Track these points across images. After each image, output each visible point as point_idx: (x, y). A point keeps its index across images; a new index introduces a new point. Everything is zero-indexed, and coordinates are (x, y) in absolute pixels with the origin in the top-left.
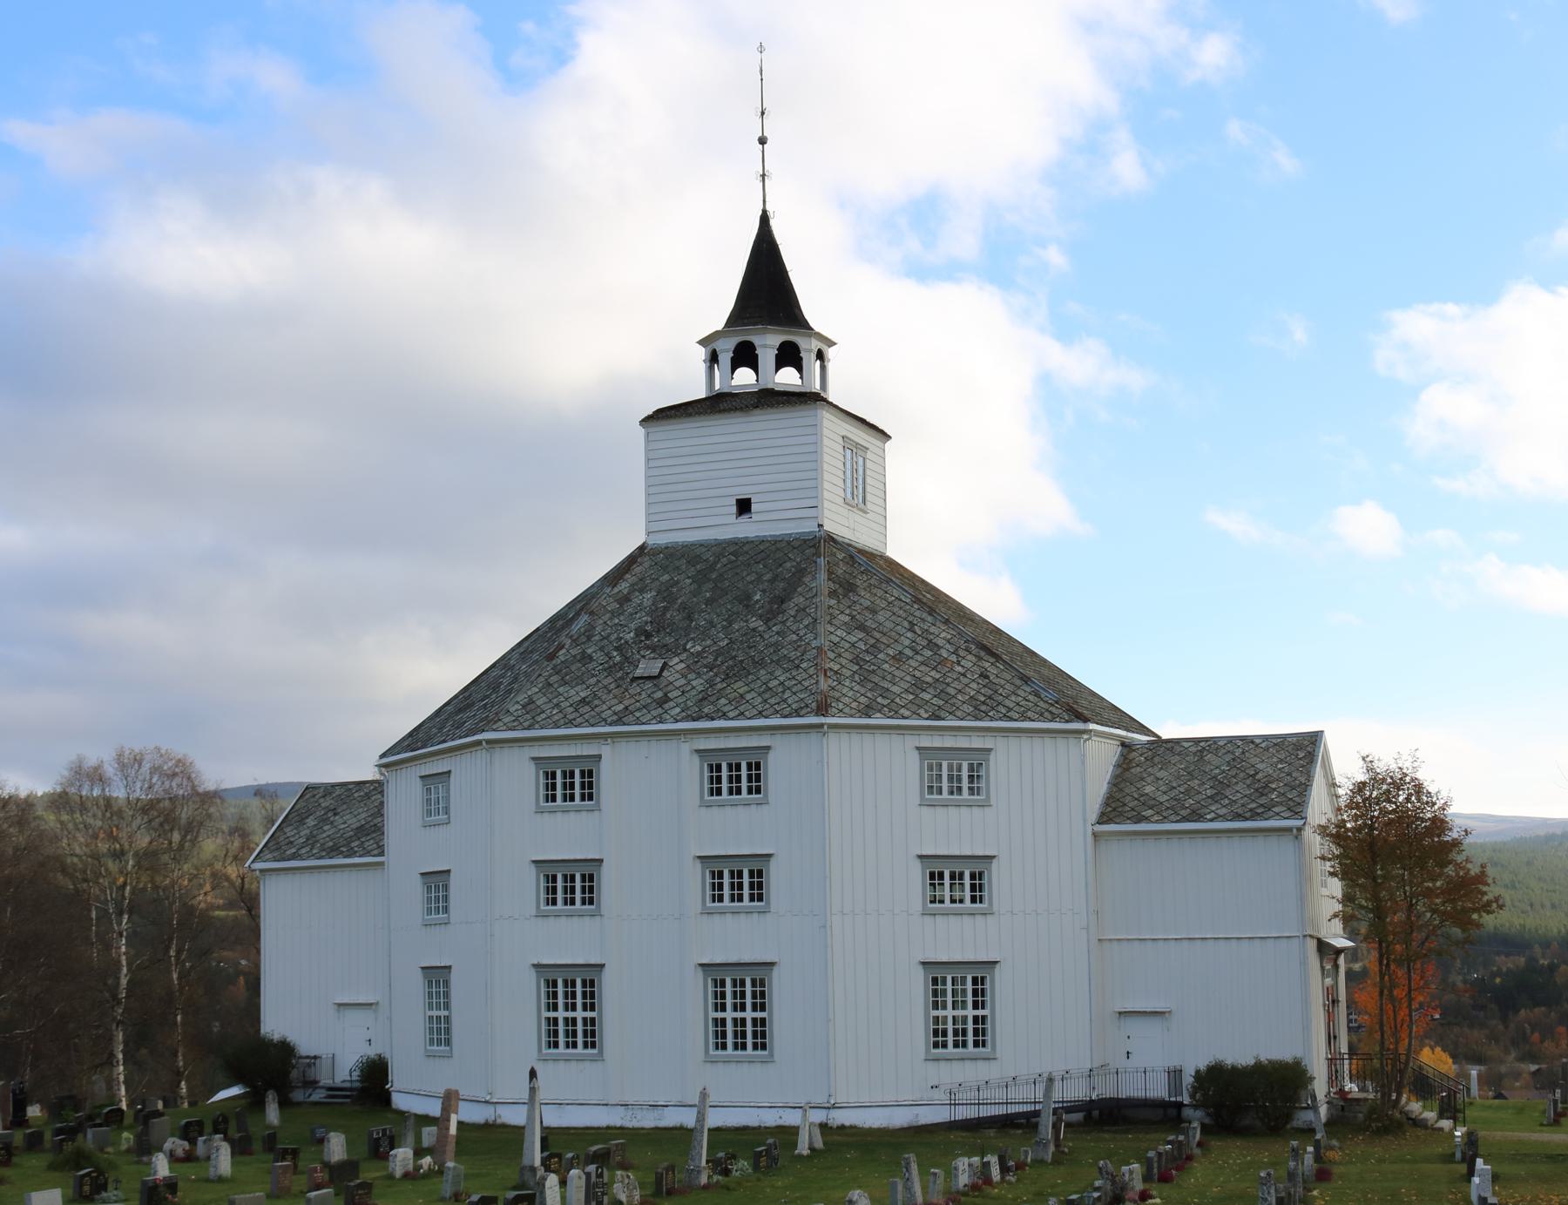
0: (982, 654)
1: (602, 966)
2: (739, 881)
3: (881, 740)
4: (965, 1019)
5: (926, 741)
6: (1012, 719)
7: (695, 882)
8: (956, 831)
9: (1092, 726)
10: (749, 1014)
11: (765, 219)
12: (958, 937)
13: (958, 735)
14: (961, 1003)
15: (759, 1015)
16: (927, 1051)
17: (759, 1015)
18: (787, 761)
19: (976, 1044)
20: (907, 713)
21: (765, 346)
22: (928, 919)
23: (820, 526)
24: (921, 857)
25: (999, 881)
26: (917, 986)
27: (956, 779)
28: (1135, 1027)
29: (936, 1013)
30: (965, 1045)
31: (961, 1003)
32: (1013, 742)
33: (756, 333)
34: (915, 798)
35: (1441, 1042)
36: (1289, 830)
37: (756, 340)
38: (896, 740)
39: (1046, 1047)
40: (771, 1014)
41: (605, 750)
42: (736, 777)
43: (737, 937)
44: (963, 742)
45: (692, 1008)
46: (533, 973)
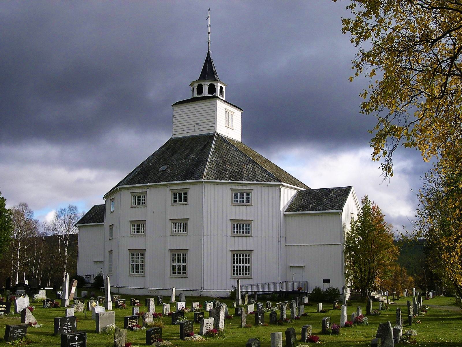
0: (254, 164)
1: (145, 250)
2: (180, 226)
3: (220, 187)
4: (243, 266)
5: (353, 192)
6: (259, 181)
7: (169, 226)
8: (241, 213)
9: (283, 183)
10: (182, 264)
11: (209, 53)
12: (241, 244)
13: (243, 186)
14: (241, 262)
15: (236, 265)
16: (231, 275)
17: (236, 265)
18: (193, 192)
19: (246, 274)
20: (260, 180)
21: (205, 85)
22: (233, 238)
23: (216, 131)
24: (231, 220)
25: (254, 227)
26: (229, 257)
27: (242, 198)
28: (295, 270)
29: (234, 265)
30: (243, 274)
31: (241, 262)
32: (259, 188)
33: (214, 82)
34: (229, 203)
35: (16, 283)
36: (338, 213)
37: (203, 83)
38: (225, 187)
39: (266, 274)
40: (144, 264)
41: (148, 190)
42: (181, 197)
43: (179, 242)
44: (244, 188)
45: (227, 263)
46: (128, 252)
